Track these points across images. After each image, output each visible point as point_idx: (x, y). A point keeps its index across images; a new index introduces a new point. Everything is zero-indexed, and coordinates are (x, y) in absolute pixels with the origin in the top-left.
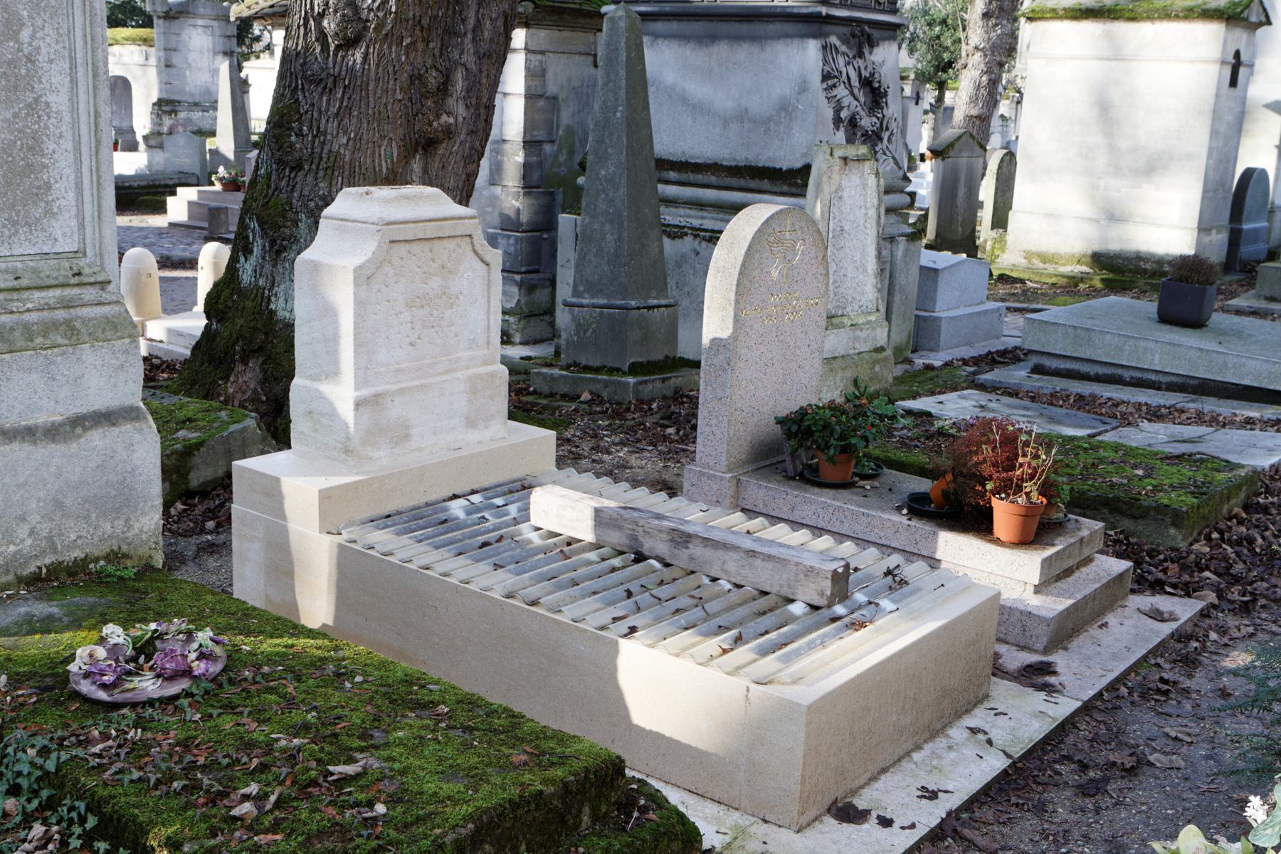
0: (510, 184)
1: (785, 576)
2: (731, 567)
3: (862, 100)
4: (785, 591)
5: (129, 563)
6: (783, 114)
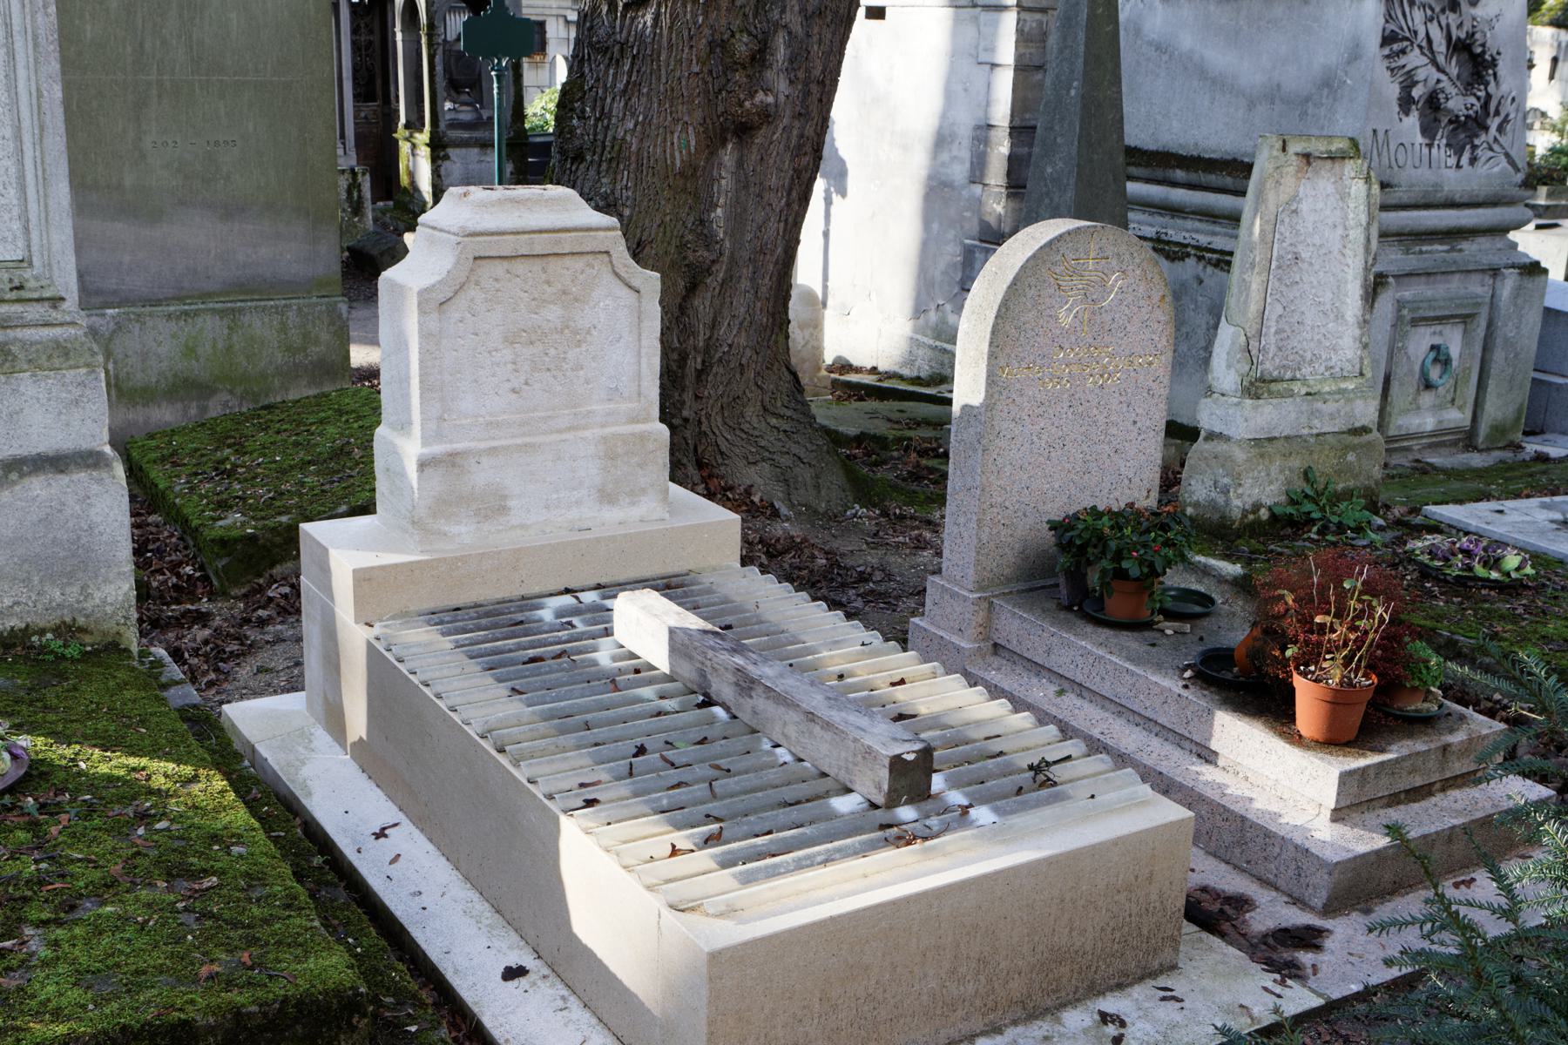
0: (993, 182)
1: (843, 754)
2: (792, 731)
3: (1454, 70)
4: (843, 777)
5: (87, 639)
6: (1326, 91)
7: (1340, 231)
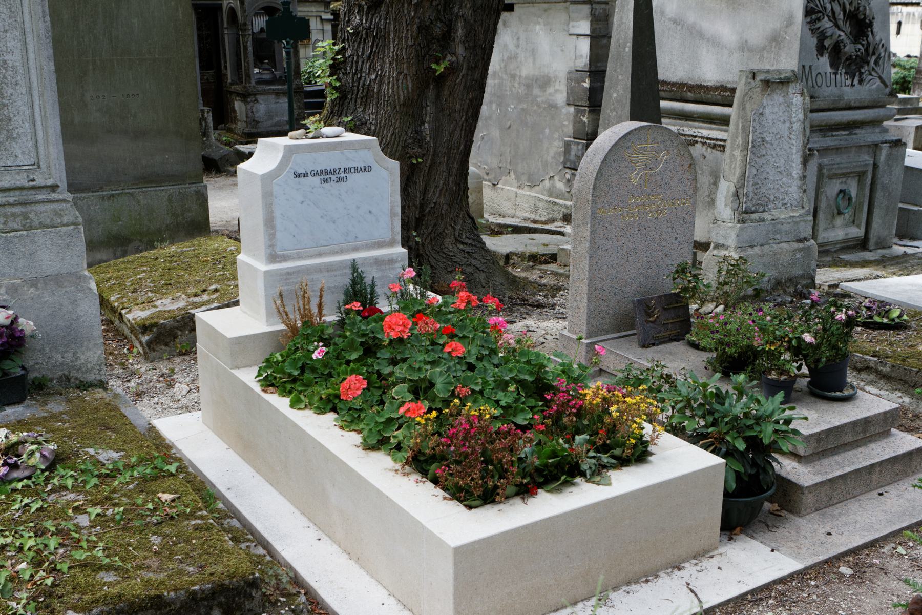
3: (848, 29)
7: (788, 124)
